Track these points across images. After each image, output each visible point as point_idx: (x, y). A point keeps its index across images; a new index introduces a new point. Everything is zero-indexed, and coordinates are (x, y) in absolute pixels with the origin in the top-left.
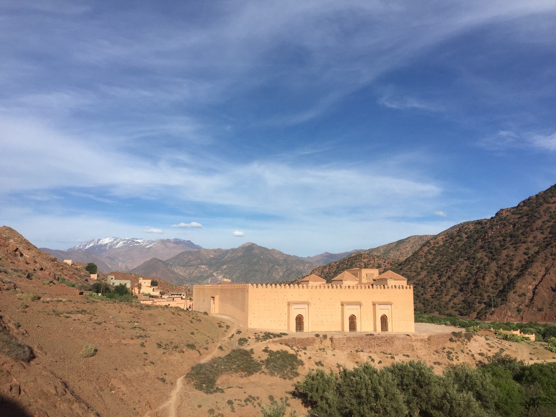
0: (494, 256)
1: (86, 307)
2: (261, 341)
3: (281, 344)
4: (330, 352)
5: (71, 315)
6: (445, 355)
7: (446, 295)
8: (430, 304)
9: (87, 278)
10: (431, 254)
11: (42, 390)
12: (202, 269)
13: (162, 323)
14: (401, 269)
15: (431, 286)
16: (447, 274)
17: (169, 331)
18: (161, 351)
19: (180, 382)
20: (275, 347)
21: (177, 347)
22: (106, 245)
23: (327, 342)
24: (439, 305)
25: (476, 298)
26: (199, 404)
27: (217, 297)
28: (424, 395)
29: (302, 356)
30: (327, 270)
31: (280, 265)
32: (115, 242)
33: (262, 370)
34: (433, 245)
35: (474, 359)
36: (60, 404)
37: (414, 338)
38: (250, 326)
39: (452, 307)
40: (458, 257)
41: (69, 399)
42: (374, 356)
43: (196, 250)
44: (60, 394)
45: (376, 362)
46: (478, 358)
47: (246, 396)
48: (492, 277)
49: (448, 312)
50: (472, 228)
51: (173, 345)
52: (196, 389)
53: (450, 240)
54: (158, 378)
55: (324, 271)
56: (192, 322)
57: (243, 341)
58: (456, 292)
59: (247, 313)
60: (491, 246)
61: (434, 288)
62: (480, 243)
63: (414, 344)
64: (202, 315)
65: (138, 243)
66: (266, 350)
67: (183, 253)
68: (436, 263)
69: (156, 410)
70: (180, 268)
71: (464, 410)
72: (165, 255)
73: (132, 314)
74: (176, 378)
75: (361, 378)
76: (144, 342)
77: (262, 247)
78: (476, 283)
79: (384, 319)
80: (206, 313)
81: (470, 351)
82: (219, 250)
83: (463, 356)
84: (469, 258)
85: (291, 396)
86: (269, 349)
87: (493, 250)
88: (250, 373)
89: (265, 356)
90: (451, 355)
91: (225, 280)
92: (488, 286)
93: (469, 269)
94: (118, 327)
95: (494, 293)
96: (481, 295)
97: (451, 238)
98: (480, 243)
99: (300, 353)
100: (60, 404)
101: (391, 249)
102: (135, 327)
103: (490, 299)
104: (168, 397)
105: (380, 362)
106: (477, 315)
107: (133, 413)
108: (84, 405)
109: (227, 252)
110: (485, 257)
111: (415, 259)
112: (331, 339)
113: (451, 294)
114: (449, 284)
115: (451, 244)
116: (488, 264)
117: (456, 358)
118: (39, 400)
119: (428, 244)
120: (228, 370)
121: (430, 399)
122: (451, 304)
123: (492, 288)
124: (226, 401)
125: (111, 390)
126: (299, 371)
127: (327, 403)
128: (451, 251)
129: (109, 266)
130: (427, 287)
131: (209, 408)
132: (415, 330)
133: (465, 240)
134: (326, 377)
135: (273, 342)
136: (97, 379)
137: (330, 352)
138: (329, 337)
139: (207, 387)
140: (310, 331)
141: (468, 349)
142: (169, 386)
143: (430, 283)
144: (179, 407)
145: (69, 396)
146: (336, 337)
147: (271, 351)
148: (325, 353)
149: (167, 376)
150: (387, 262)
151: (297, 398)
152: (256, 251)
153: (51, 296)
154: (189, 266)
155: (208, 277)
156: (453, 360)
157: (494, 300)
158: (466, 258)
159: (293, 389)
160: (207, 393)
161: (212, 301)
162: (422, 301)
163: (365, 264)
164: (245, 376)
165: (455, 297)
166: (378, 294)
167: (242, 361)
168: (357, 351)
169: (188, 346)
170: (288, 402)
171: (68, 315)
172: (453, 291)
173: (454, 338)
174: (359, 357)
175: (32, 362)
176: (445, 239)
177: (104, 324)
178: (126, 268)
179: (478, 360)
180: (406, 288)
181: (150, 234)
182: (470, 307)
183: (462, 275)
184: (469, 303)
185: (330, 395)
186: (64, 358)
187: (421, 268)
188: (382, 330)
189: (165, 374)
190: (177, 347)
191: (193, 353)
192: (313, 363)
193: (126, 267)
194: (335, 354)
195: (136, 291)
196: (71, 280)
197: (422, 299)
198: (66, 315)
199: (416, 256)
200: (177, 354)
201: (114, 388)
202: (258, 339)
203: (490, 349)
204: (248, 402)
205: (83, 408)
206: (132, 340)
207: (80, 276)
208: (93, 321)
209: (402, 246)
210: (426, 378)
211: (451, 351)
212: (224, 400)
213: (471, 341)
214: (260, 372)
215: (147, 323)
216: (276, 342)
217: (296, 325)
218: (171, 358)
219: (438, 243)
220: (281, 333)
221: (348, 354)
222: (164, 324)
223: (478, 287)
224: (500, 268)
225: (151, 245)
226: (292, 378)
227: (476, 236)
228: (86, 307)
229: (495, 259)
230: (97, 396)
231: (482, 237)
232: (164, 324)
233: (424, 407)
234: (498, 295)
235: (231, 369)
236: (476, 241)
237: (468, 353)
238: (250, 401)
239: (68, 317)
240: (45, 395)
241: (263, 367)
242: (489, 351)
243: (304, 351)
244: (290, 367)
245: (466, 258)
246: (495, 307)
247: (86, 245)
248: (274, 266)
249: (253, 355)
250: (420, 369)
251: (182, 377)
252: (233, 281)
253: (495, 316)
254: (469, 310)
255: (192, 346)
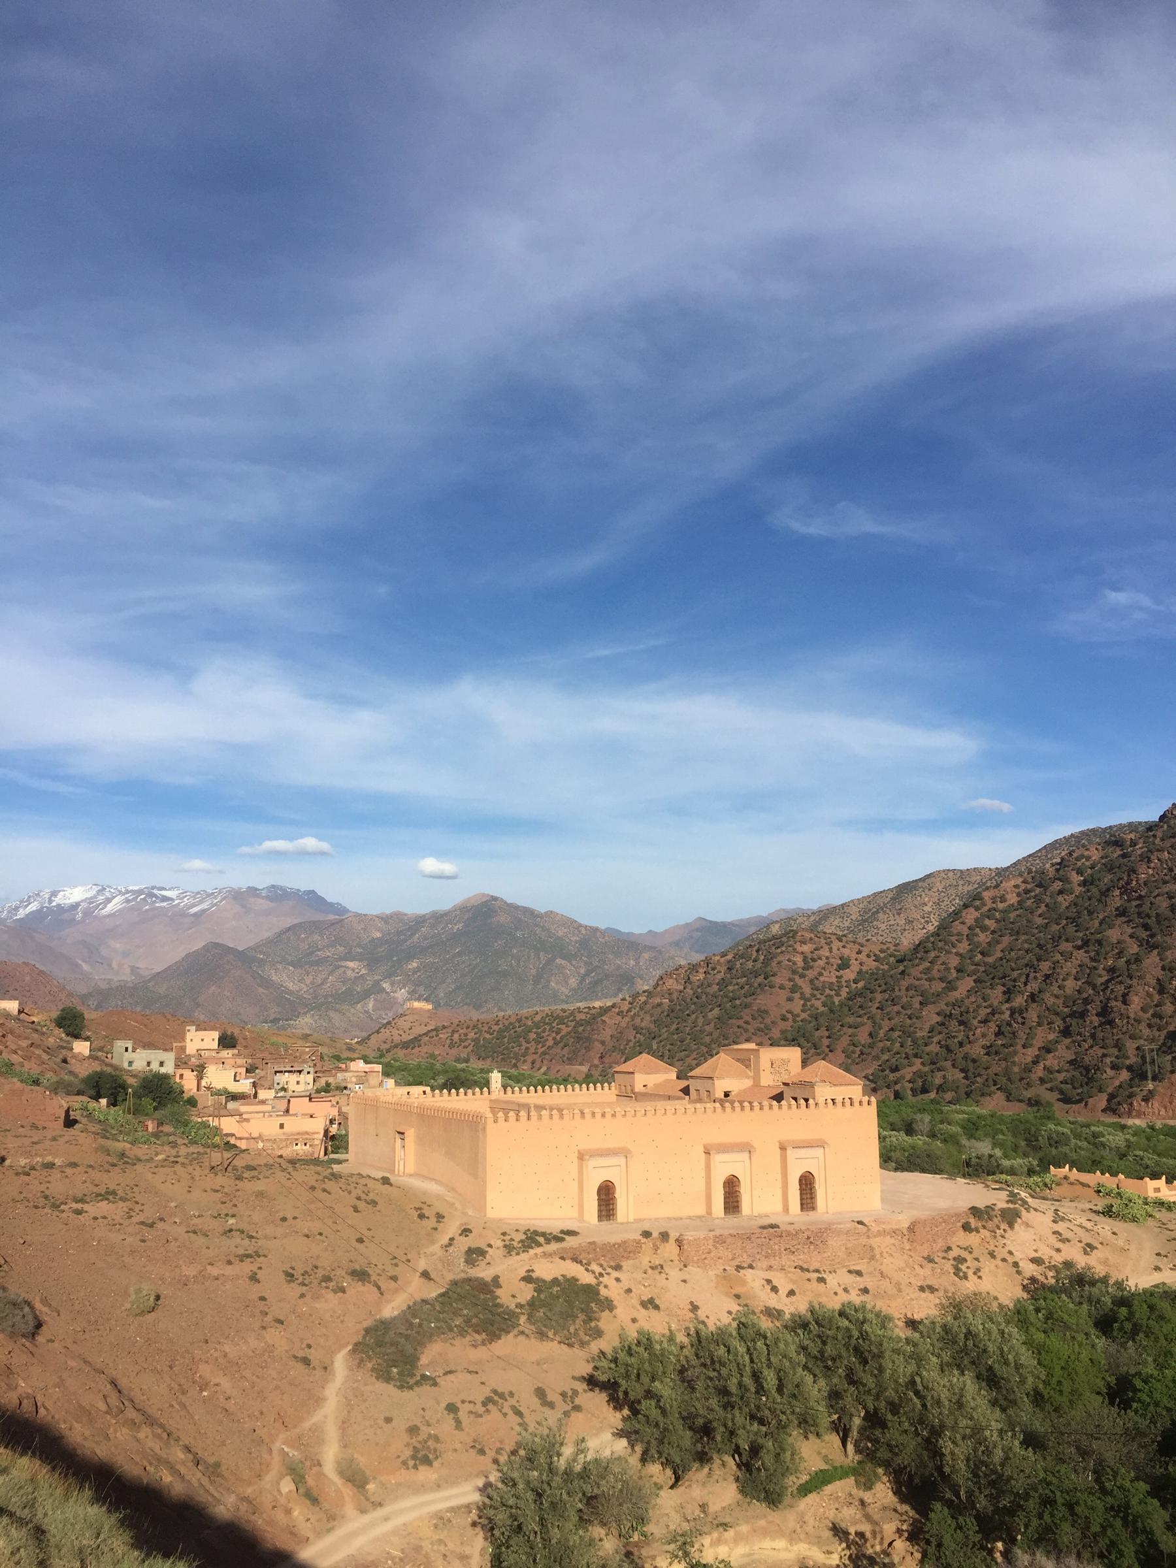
0: (1153, 936)
1: (113, 1179)
2: (518, 1254)
3: (563, 1258)
4: (674, 1274)
5: (86, 1207)
6: (948, 1266)
7: (1024, 1047)
8: (983, 1072)
9: (64, 1052)
10: (984, 929)
11: (80, 1406)
12: (349, 973)
13: (289, 1216)
14: (903, 973)
15: (985, 1022)
16: (1028, 988)
17: (307, 1236)
18: (294, 1290)
19: (341, 1362)
20: (548, 1270)
21: (327, 1279)
22: (74, 907)
23: (670, 1249)
24: (1007, 1073)
25: (1104, 1055)
26: (388, 1415)
27: (411, 1134)
28: (870, 1382)
29: (611, 1289)
30: (702, 976)
31: (568, 957)
32: (101, 898)
33: (521, 1328)
34: (989, 905)
35: (1019, 1273)
36: (116, 1431)
37: (875, 1228)
38: (491, 1214)
39: (1042, 1080)
40: (1056, 940)
41: (133, 1420)
42: (779, 1280)
43: (331, 917)
44: (115, 1410)
45: (783, 1292)
46: (1029, 1269)
47: (486, 1392)
48: (1149, 995)
49: (1028, 1094)
50: (1095, 855)
51: (320, 1273)
52: (377, 1378)
53: (1038, 890)
54: (295, 1357)
55: (694, 979)
56: (356, 1210)
57: (475, 1255)
58: (1051, 1037)
59: (485, 1182)
60: (1146, 908)
61: (993, 1027)
62: (1116, 899)
63: (874, 1242)
64: (378, 1185)
65: (165, 899)
66: (528, 1279)
67: (295, 926)
68: (999, 955)
69: (298, 1430)
70: (285, 982)
71: (951, 1413)
72: (242, 935)
73: (219, 1195)
74: (332, 1353)
75: (729, 1351)
76: (255, 1269)
77: (517, 907)
78: (1104, 1012)
79: (807, 1183)
80: (386, 1181)
81: (1010, 1253)
82: (398, 916)
83: (993, 1267)
84: (1086, 943)
85: (585, 1386)
86: (534, 1275)
87: (1152, 922)
88: (494, 1337)
89: (526, 1293)
90: (963, 1267)
91: (416, 1004)
92: (1138, 1021)
93: (1086, 974)
94: (195, 1232)
95: (1153, 1040)
96: (1118, 1045)
97: (1039, 885)
98: (1116, 899)
99: (605, 1280)
100: (116, 1431)
101: (881, 909)
102: (231, 1231)
103: (1143, 1057)
104: (319, 1401)
105: (791, 1293)
106: (1109, 1101)
107: (253, 1441)
108: (159, 1431)
109: (420, 921)
110: (1129, 940)
111: (941, 944)
112: (679, 1242)
113: (1038, 1042)
114: (1033, 1015)
115: (1038, 900)
116: (1138, 960)
117: (975, 1273)
118: (76, 1425)
119: (977, 903)
120: (446, 1329)
121: (882, 1389)
122: (1039, 1071)
123: (1150, 1026)
124: (444, 1405)
125: (201, 1390)
126: (602, 1325)
127: (658, 1406)
128: (1039, 921)
129: (86, 967)
130: (975, 1022)
131: (411, 1424)
132: (884, 1200)
133: (1078, 890)
134: (658, 1347)
135: (545, 1255)
136: (171, 1367)
137: (674, 1274)
138: (674, 1235)
139: (400, 1374)
140: (631, 1219)
141: (1007, 1248)
142: (319, 1373)
143: (983, 1012)
144: (343, 1422)
145: (131, 1414)
146: (689, 1236)
147: (539, 1280)
148: (663, 1275)
149: (312, 1351)
150: (865, 950)
151: (597, 1390)
152: (502, 918)
153: (28, 1154)
154: (312, 964)
155: (366, 995)
156: (966, 1277)
157: (1153, 1062)
158: (1080, 943)
159: (586, 1369)
160: (401, 1387)
161: (399, 1141)
162: (961, 1063)
163: (805, 959)
164: (483, 1343)
165: (1049, 1051)
166: (790, 1121)
167: (474, 1308)
168: (739, 1268)
169: (354, 1273)
170: (577, 1401)
171: (79, 1206)
172: (1044, 1035)
173: (973, 1222)
174: (744, 1283)
175: (40, 1339)
176: (1023, 886)
177: (160, 1225)
178: (132, 973)
179: (1028, 1275)
180: (861, 1103)
181: (197, 876)
182: (1090, 1080)
183: (1069, 991)
184: (1087, 1069)
185: (666, 1389)
186: (96, 1321)
187: (959, 971)
188: (802, 1209)
189: (309, 1346)
190: (327, 1279)
191: (365, 1291)
192: (635, 1302)
193: (134, 969)
194: (686, 1277)
195: (188, 1082)
196: (27, 1065)
197: (960, 1056)
198: (75, 1206)
199: (944, 933)
200: (331, 1295)
201: (207, 1384)
202: (509, 1249)
203: (1059, 1245)
204: (490, 1406)
205: (159, 1437)
206: (230, 1267)
207: (48, 1050)
208: (135, 1219)
209: (909, 901)
210: (871, 1343)
211: (964, 1254)
212: (438, 1403)
213: (1016, 1226)
214: (515, 1331)
215: (257, 1216)
216: (550, 1255)
217: (599, 1205)
218: (318, 1306)
219: (1003, 899)
220: (562, 1232)
221: (717, 1276)
222: (295, 1218)
223: (1111, 1023)
224: (1171, 970)
225: (205, 906)
226: (588, 1343)
227: (1108, 878)
228: (113, 1179)
229: (1155, 946)
230: (177, 1406)
231: (1122, 883)
232: (295, 1218)
233: (871, 1407)
234: (1164, 1044)
235: (451, 1330)
236: (1106, 893)
237: (1004, 1260)
238: (495, 1403)
239: (79, 1212)
240: (86, 1414)
241: (523, 1319)
242: (1058, 1250)
243: (615, 1274)
244: (582, 1316)
245: (1080, 943)
246: (1154, 1079)
247: (17, 909)
248: (550, 961)
249: (499, 1292)
250: (862, 1323)
251: (345, 1351)
252: (437, 1005)
253: (1156, 1105)
254: (1086, 1088)
255: (361, 1275)
